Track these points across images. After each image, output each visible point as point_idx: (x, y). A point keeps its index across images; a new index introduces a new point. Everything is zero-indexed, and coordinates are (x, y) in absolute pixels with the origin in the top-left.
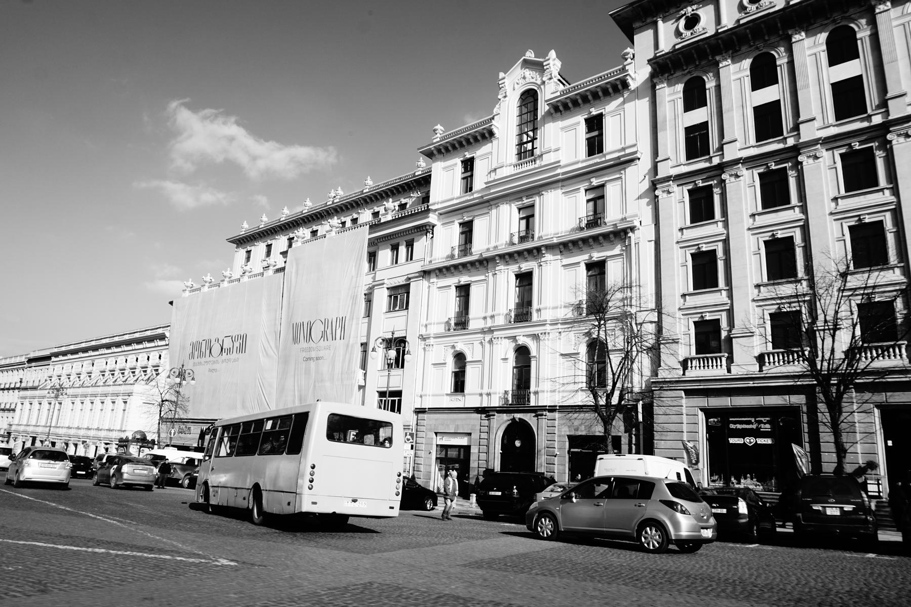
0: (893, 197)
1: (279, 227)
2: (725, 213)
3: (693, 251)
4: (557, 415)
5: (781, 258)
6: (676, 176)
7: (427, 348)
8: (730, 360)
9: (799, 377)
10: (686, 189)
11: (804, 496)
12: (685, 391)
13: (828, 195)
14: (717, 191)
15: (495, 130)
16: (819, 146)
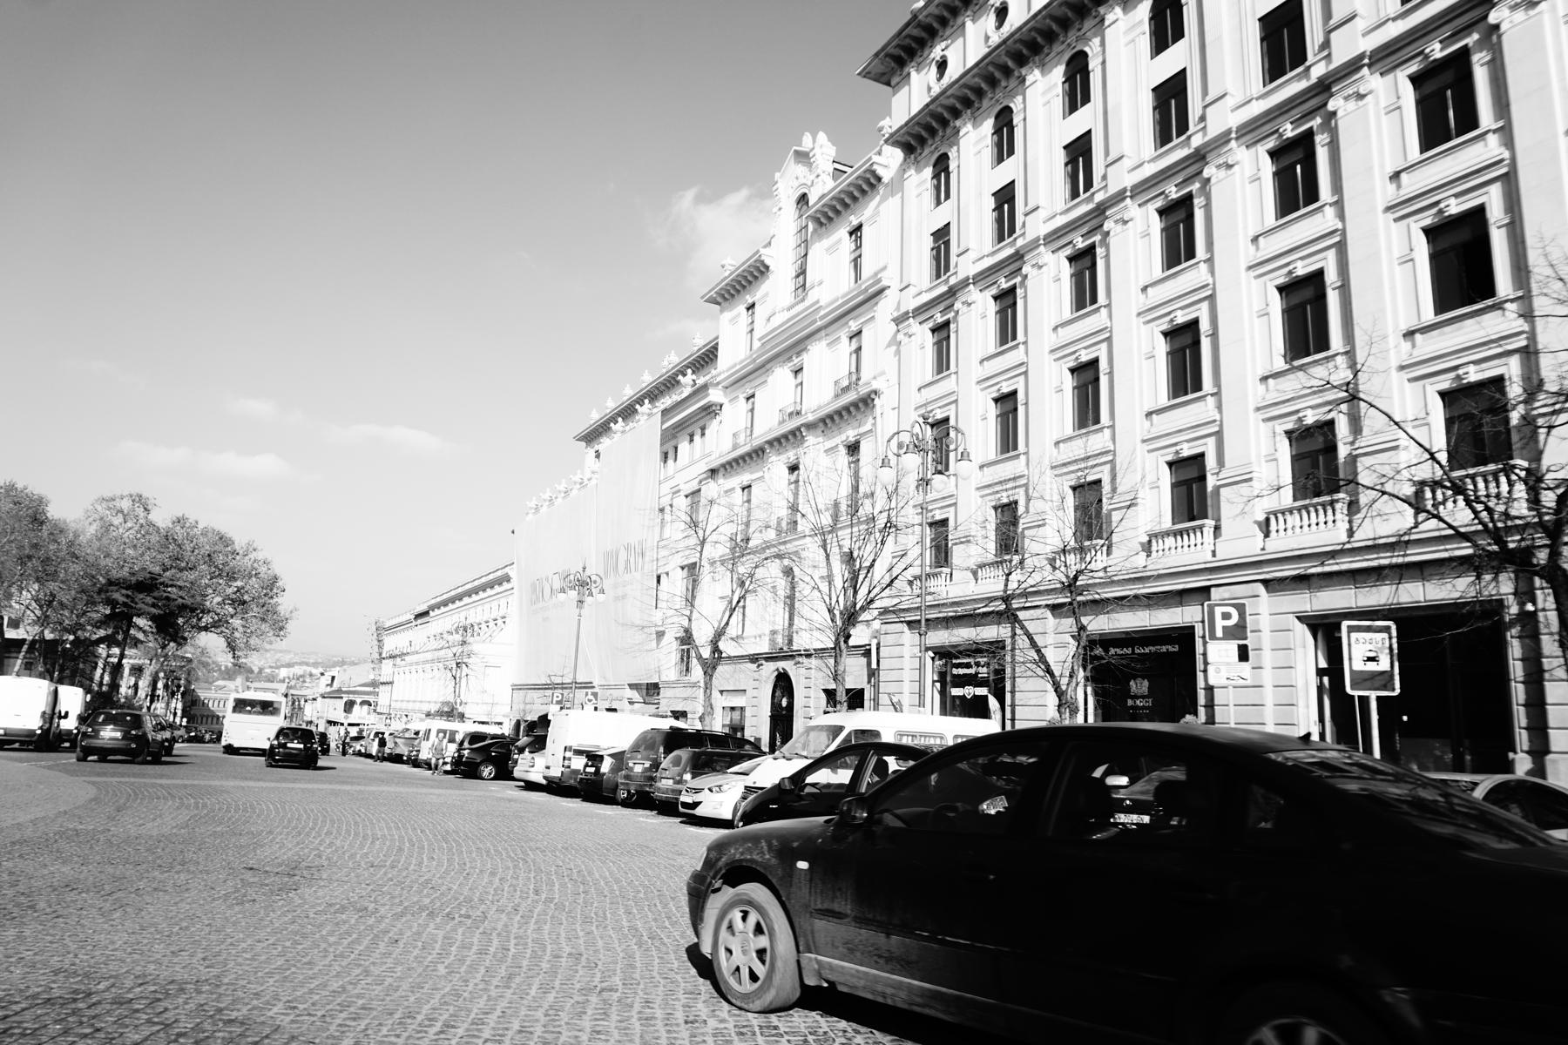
0: (1503, 149)
1: (595, 430)
2: (1337, 187)
3: (1428, 222)
4: (814, 662)
5: (1307, 313)
6: (1134, 187)
7: (1423, 415)
8: (1353, 507)
9: (1333, 554)
10: (1262, 150)
11: (1106, 774)
12: (1265, 582)
13: (1382, 166)
14: (1321, 140)
15: (767, 262)
16: (1365, 70)
